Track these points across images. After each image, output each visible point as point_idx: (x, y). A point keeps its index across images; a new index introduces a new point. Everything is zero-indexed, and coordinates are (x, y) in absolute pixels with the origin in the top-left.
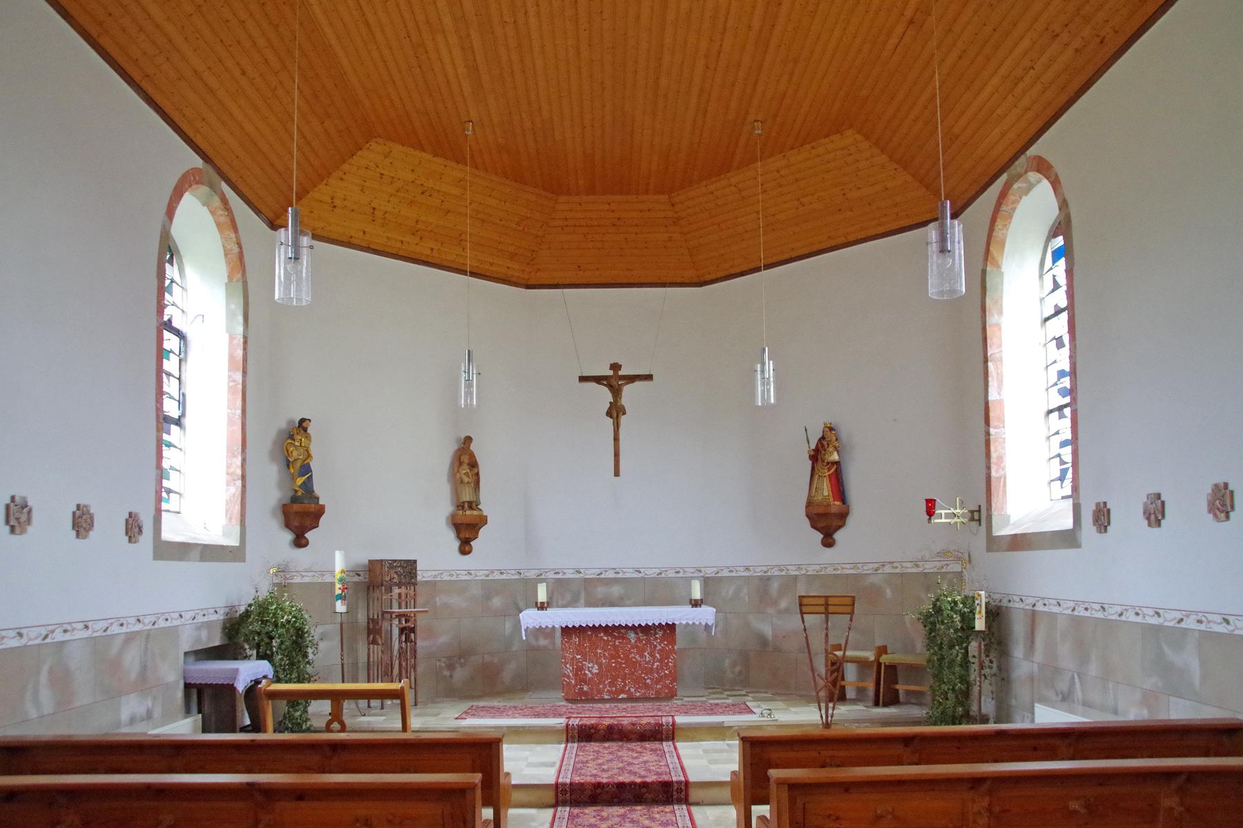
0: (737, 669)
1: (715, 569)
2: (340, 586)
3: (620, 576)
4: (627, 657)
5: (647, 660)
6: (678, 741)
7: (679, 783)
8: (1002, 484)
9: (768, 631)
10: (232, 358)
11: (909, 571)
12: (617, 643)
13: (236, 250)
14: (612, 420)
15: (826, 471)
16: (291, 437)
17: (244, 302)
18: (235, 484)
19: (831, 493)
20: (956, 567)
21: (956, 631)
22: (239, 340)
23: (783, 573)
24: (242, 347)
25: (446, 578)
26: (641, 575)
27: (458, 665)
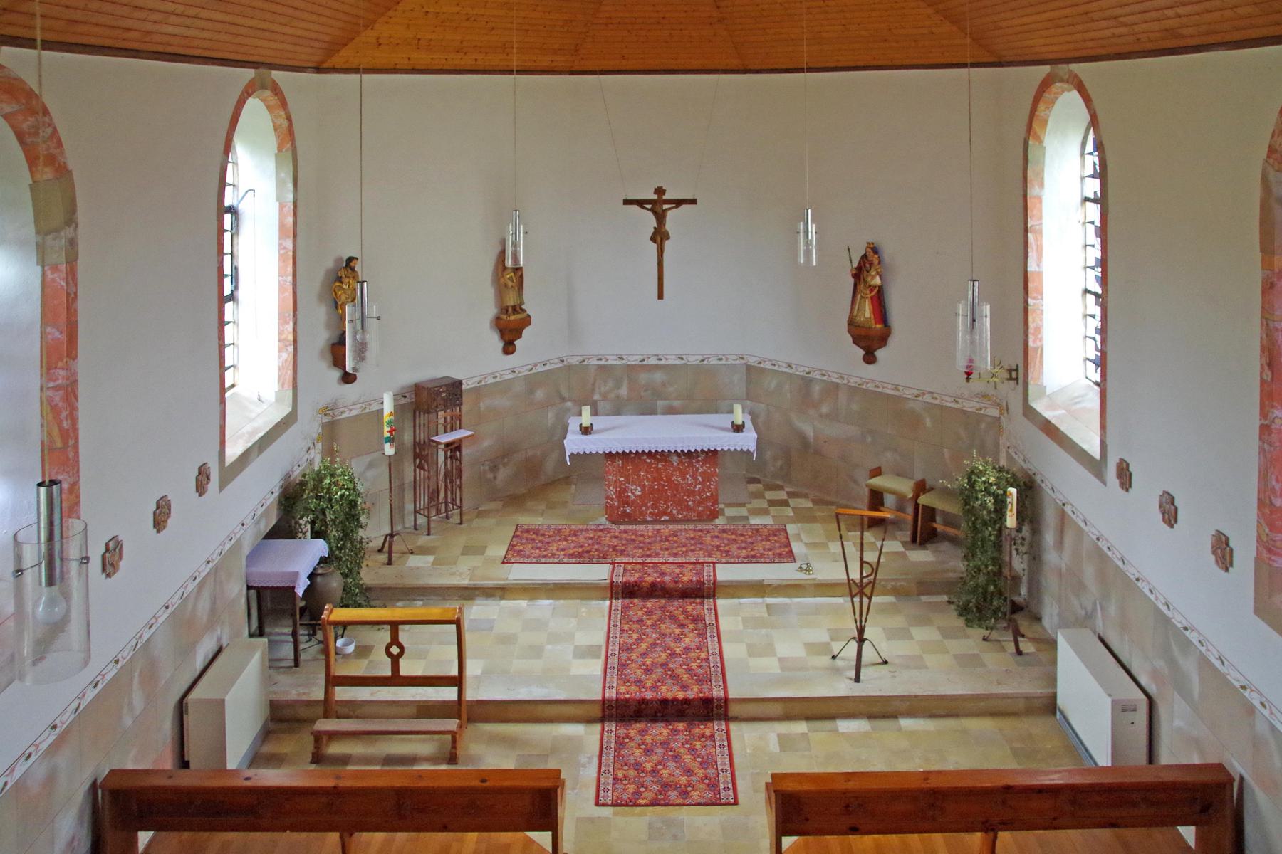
0: (779, 463)
1: (758, 359)
2: (389, 429)
3: (663, 362)
4: (669, 480)
5: (690, 482)
6: (719, 598)
7: (719, 699)
8: (1039, 355)
9: (809, 431)
10: (282, 226)
11: (949, 405)
12: (660, 466)
13: (286, 124)
14: (656, 245)
15: (868, 292)
16: (339, 279)
17: (293, 166)
18: (287, 350)
19: (873, 316)
20: (994, 412)
21: (989, 512)
22: (289, 207)
23: (825, 378)
24: (292, 214)
25: (490, 380)
26: (683, 362)
27: (501, 466)
